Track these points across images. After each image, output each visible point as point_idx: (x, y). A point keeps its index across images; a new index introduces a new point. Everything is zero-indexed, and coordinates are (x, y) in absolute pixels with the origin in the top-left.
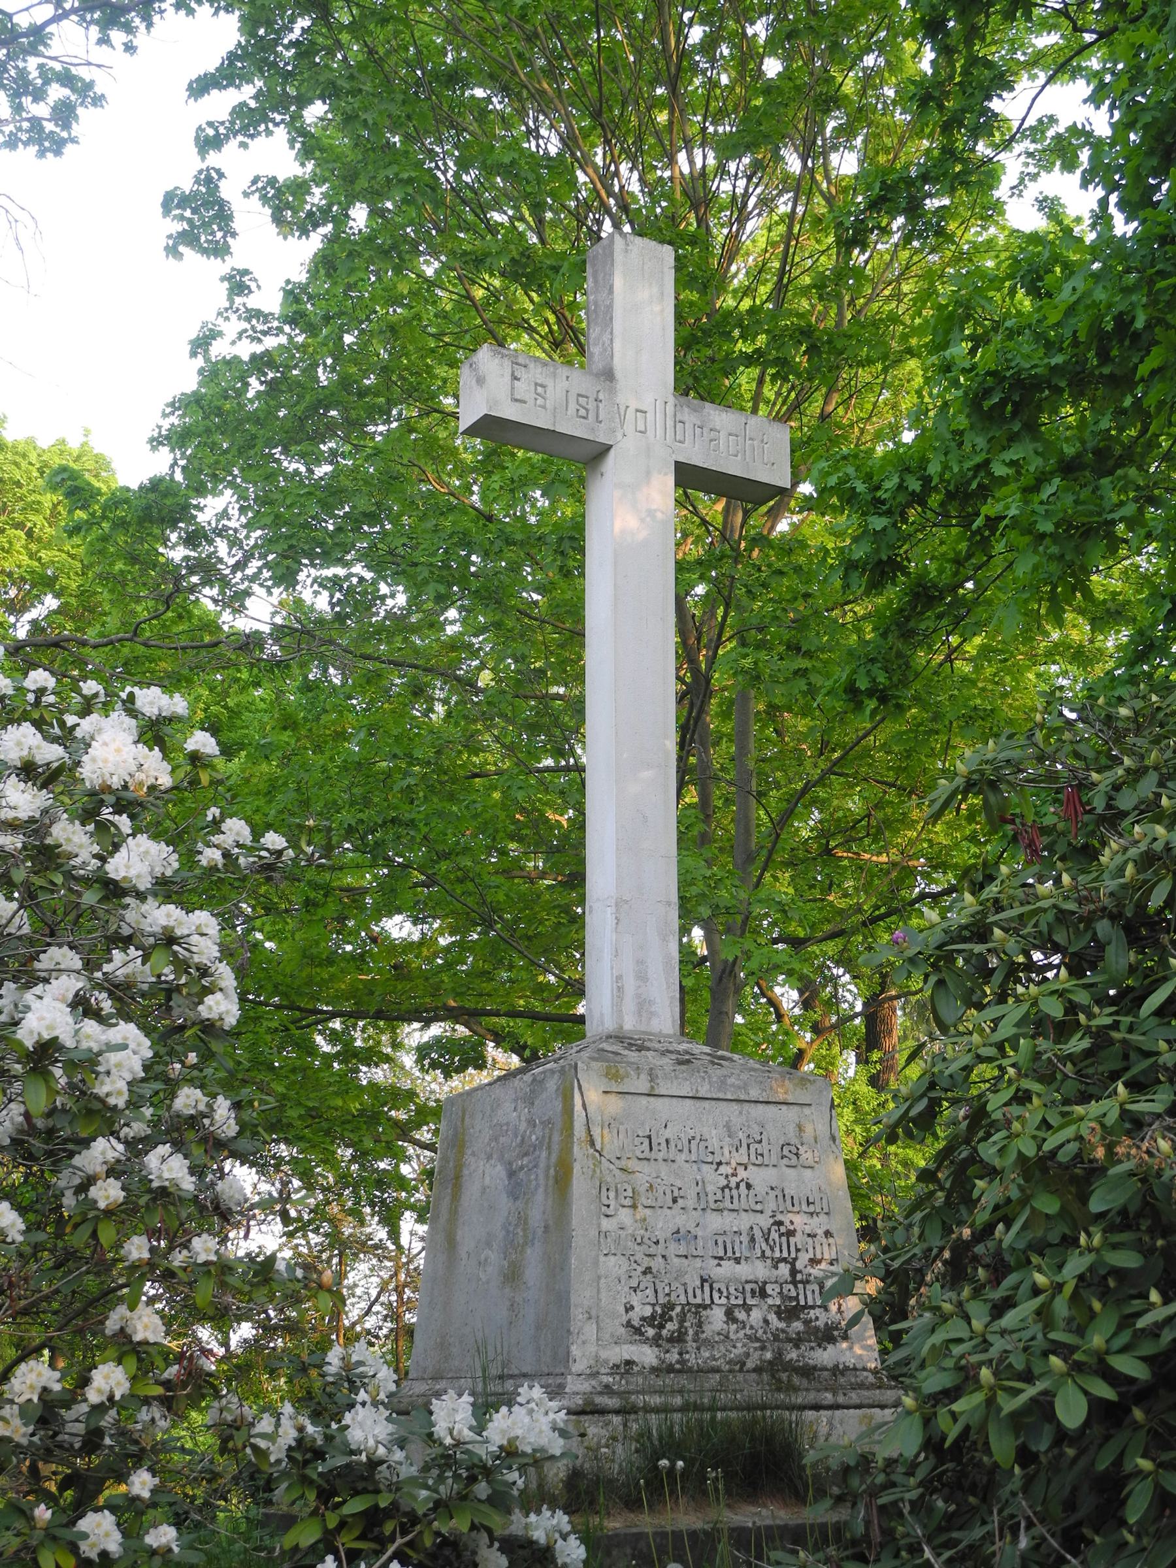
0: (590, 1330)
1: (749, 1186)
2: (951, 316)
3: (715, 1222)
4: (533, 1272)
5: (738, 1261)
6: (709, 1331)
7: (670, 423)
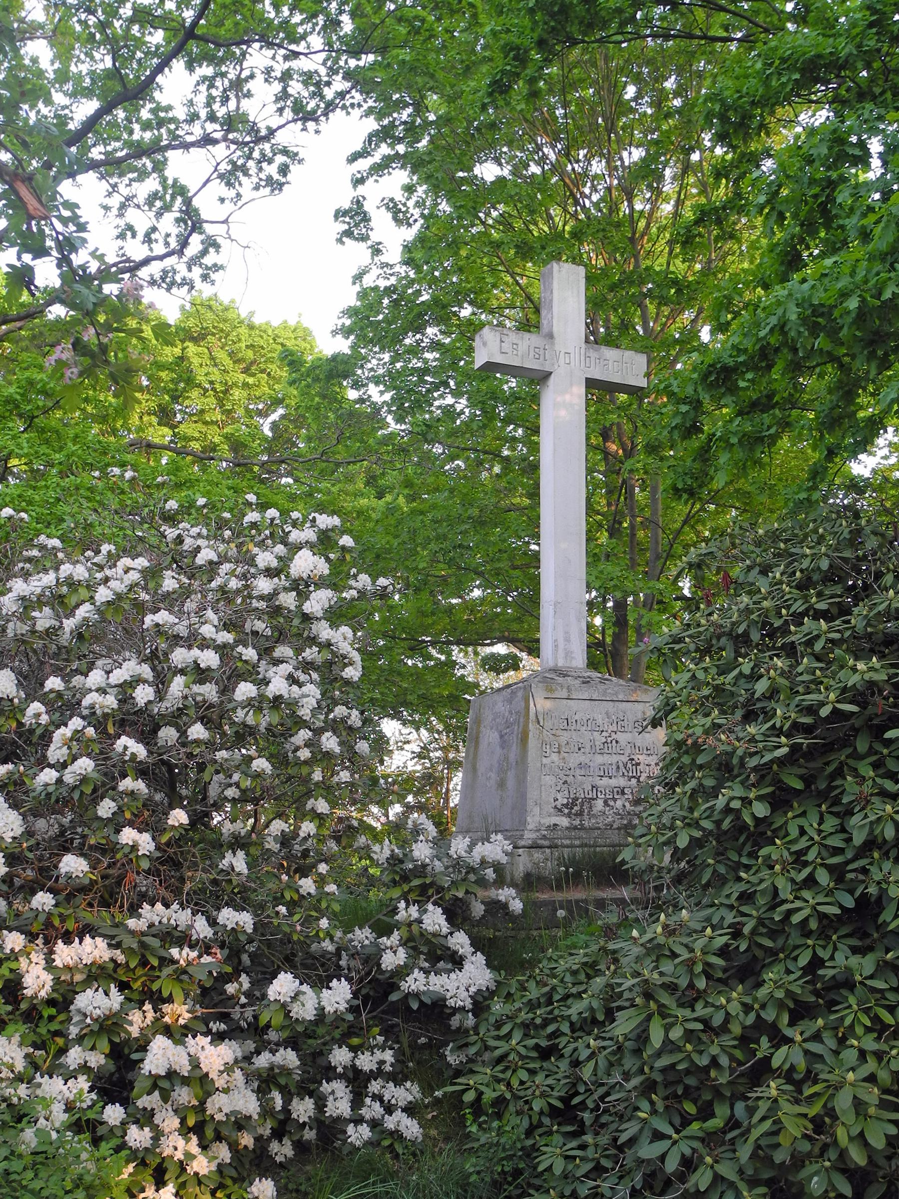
0: (537, 810)
1: (617, 742)
2: (721, 303)
3: (599, 759)
4: (511, 783)
5: (610, 778)
6: (595, 811)
7: (583, 358)
